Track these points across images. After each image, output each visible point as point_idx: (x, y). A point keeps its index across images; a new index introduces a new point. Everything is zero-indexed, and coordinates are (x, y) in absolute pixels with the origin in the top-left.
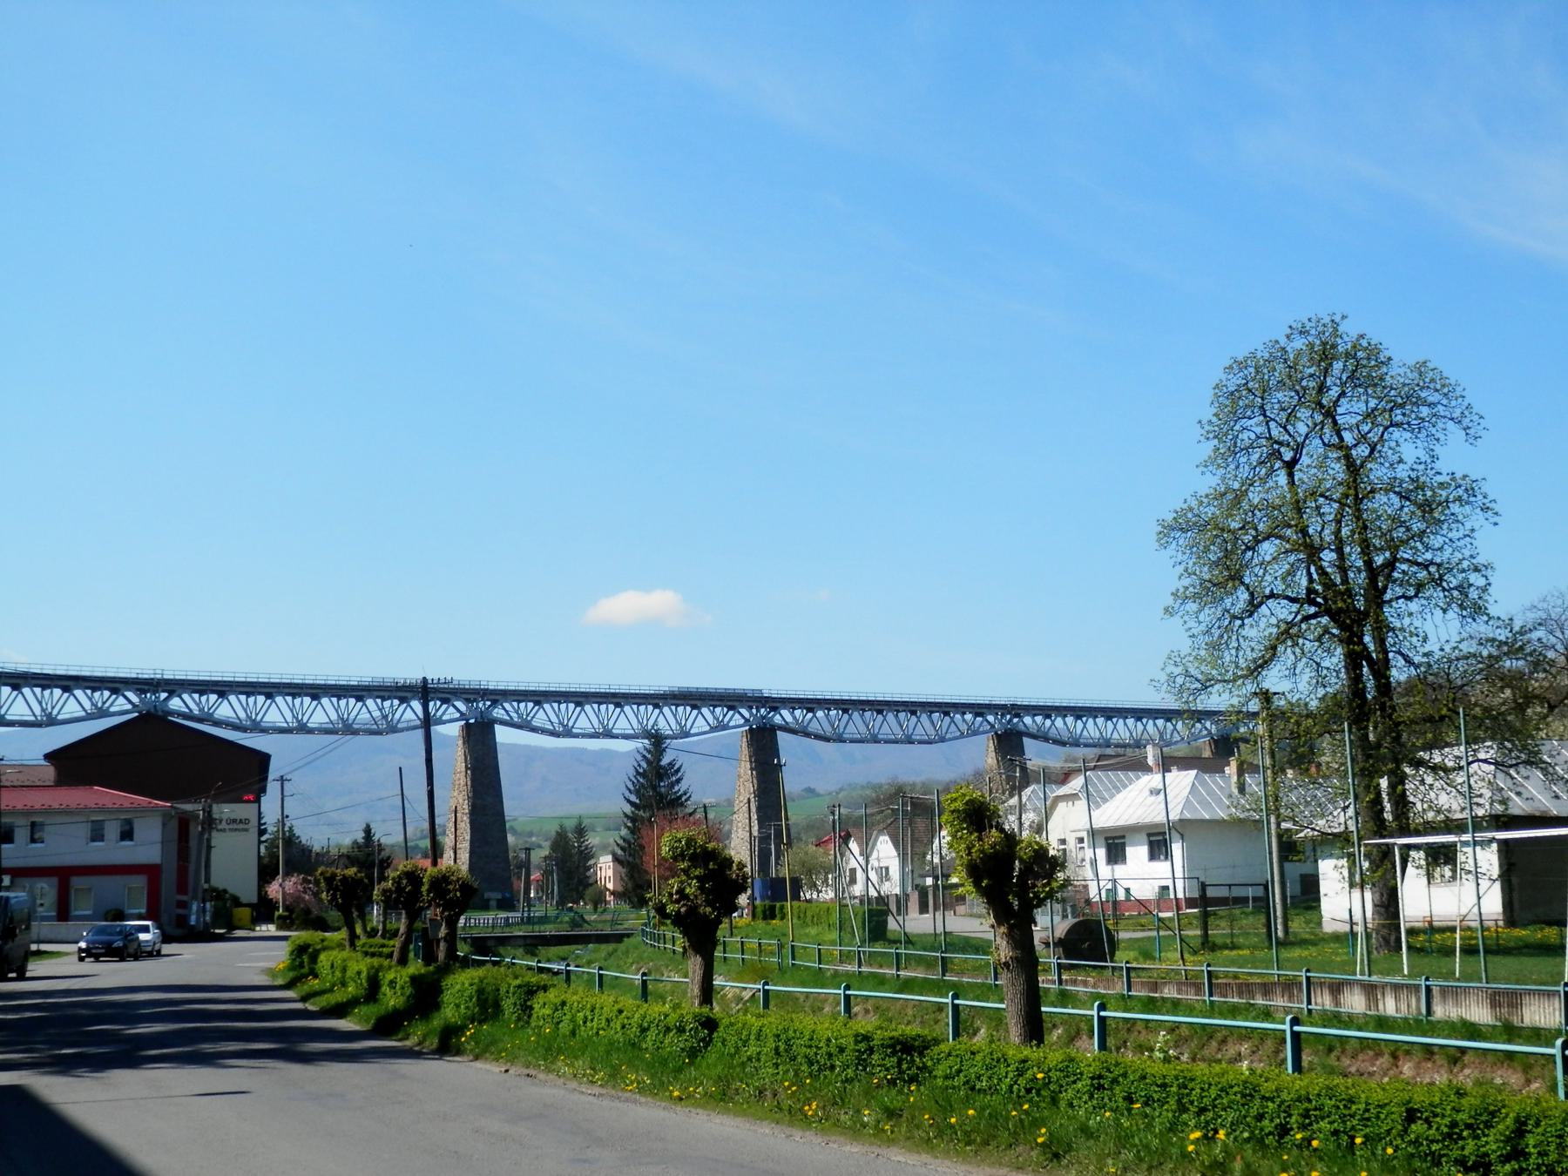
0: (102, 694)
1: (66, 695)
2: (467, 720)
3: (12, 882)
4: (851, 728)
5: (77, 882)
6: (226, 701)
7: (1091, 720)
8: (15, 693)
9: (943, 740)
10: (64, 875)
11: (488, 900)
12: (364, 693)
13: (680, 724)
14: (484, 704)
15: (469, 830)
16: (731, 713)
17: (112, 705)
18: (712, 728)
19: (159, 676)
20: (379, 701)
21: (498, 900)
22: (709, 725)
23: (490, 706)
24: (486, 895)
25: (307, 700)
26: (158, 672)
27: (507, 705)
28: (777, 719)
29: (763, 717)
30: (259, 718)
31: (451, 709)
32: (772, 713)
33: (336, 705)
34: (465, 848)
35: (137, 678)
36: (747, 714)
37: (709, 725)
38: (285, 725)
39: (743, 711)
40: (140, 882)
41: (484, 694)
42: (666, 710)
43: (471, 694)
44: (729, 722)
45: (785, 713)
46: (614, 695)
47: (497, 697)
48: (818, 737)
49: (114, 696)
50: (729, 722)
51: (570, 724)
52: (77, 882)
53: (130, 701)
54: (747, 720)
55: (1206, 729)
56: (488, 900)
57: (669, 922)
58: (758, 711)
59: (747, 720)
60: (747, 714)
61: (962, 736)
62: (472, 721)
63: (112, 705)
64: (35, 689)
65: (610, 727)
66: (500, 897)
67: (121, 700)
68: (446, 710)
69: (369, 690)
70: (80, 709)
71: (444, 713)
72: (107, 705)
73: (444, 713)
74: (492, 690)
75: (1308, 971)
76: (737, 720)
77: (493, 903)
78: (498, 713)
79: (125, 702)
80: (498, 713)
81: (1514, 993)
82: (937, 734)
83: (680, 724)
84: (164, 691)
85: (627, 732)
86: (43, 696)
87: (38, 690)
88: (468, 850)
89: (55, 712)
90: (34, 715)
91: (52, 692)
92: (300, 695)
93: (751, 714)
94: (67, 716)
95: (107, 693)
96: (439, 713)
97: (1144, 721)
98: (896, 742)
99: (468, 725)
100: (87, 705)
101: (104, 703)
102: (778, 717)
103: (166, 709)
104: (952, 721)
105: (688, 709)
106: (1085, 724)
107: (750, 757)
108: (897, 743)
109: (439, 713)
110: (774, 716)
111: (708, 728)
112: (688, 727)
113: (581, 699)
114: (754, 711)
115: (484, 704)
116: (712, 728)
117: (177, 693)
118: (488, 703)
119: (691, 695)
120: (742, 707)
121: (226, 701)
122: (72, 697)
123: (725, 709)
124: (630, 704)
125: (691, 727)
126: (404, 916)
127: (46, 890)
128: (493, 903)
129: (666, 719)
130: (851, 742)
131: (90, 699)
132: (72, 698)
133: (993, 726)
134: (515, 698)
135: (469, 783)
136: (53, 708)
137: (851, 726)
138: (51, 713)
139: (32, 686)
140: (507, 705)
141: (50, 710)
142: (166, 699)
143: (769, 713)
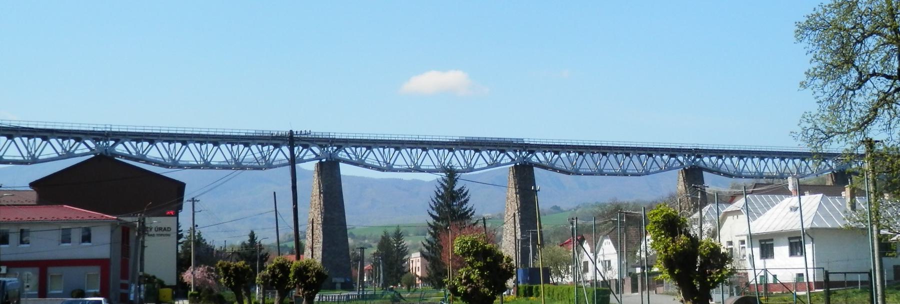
0: (69, 142)
2: (321, 160)
3: (7, 271)
5: (52, 271)
7: (749, 160)
9: (648, 173)
10: (43, 266)
11: (335, 283)
14: (332, 149)
15: (322, 235)
16: (502, 155)
17: (76, 149)
18: (489, 165)
20: (260, 146)
21: (342, 284)
22: (57, 152)
23: (336, 150)
24: (334, 280)
28: (534, 159)
29: (524, 158)
32: (530, 155)
36: (513, 156)
37: (57, 152)
39: (511, 154)
40: (95, 271)
41: (332, 141)
42: (430, 152)
45: (539, 155)
46: (422, 142)
48: (562, 171)
49: (78, 143)
52: (52, 271)
54: (513, 160)
55: (829, 166)
56: (335, 283)
59: (513, 160)
60: (513, 156)
61: (661, 170)
63: (76, 149)
65: (419, 164)
66: (343, 281)
69: (158, 136)
70: (161, 157)
72: (73, 149)
74: (337, 139)
76: (507, 160)
77: (338, 285)
78: (342, 155)
79: (85, 147)
80: (342, 155)
82: (644, 169)
84: (112, 140)
85: (430, 168)
88: (321, 249)
89: (37, 154)
90: (23, 156)
91: (35, 141)
92: (205, 142)
93: (516, 156)
95: (73, 141)
96: (499, 159)
97: (786, 160)
98: (615, 174)
102: (534, 157)
103: (113, 152)
104: (654, 160)
105: (473, 152)
106: (745, 162)
107: (515, 185)
109: (499, 159)
110: (531, 157)
112: (473, 164)
113: (398, 145)
114: (518, 153)
115: (332, 149)
116: (489, 165)
118: (335, 148)
120: (510, 151)
122: (13, 143)
123: (498, 152)
128: (338, 285)
130: (584, 175)
131: (61, 145)
132: (49, 144)
133: (682, 164)
134: (354, 144)
135: (322, 203)
136: (36, 151)
137: (371, 156)
138: (34, 155)
139: (21, 136)
140: (348, 150)
141: (33, 153)
142: (114, 145)
143: (528, 155)
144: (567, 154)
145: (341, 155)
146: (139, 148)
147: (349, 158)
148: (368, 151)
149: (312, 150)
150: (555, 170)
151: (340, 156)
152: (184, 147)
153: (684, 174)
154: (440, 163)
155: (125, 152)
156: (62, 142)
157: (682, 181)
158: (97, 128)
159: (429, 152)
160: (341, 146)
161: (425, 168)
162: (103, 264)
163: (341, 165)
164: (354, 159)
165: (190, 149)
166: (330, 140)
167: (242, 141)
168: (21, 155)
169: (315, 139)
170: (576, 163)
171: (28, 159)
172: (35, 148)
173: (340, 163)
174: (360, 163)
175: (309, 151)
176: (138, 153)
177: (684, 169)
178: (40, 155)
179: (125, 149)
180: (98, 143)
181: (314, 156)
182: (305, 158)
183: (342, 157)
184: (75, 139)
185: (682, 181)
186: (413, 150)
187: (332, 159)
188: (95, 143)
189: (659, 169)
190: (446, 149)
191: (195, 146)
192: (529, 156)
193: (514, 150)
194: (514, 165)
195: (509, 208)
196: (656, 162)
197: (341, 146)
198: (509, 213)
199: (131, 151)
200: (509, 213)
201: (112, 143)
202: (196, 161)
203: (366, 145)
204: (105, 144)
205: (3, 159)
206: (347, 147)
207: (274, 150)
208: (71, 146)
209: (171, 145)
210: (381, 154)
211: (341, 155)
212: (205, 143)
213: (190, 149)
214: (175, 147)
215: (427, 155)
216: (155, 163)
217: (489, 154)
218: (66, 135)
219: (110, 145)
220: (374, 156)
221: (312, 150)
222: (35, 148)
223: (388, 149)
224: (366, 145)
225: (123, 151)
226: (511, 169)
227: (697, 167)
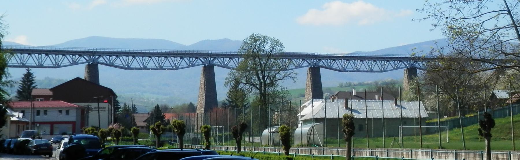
0: (76, 57)
1: (64, 57)
3: (39, 125)
4: (349, 67)
5: (55, 126)
6: (118, 59)
8: (47, 56)
9: (385, 71)
10: (52, 124)
12: (135, 55)
13: (369, 67)
14: (316, 60)
16: (401, 63)
17: (196, 62)
18: (296, 67)
19: (95, 50)
23: (318, 61)
25: (179, 59)
26: (95, 49)
27: (324, 61)
28: (417, 65)
29: (412, 64)
30: (130, 65)
31: (403, 64)
32: (415, 63)
33: (55, 58)
34: (203, 110)
35: (88, 51)
38: (156, 67)
39: (405, 62)
40: (70, 126)
41: (211, 55)
42: (378, 62)
43: (206, 55)
44: (400, 66)
47: (215, 57)
48: (337, 70)
49: (80, 57)
50: (400, 66)
51: (162, 65)
52: (55, 126)
53: (86, 59)
54: (309, 64)
57: (121, 126)
58: (410, 62)
60: (406, 64)
61: (394, 69)
62: (206, 65)
63: (196, 62)
64: (53, 55)
65: (359, 68)
67: (82, 58)
68: (401, 64)
69: (50, 52)
71: (400, 65)
72: (77, 60)
73: (400, 65)
75: (456, 151)
76: (403, 65)
78: (321, 63)
79: (84, 59)
80: (321, 63)
81: (447, 152)
83: (369, 67)
84: (97, 55)
86: (297, 61)
87: (54, 55)
90: (53, 64)
92: (160, 57)
93: (408, 64)
94: (182, 67)
96: (399, 65)
98: (367, 72)
99: (205, 66)
100: (188, 63)
101: (76, 60)
102: (417, 64)
103: (97, 62)
105: (386, 62)
107: (310, 77)
108: (354, 72)
109: (399, 65)
110: (416, 64)
111: (69, 64)
113: (134, 55)
114: (409, 62)
116: (71, 63)
117: (82, 56)
119: (291, 55)
120: (85, 55)
121: (118, 59)
123: (399, 62)
124: (379, 60)
125: (61, 64)
126: (178, 137)
127: (48, 129)
129: (31, 60)
131: (72, 59)
133: (406, 66)
134: (173, 56)
136: (59, 62)
138: (58, 63)
139: (69, 55)
140: (324, 61)
141: (58, 62)
142: (213, 60)
143: (414, 63)
144: (394, 61)
145: (216, 62)
146: (74, 58)
147: (419, 67)
148: (134, 58)
149: (84, 58)
150: (333, 69)
151: (215, 63)
152: (182, 59)
153: (407, 71)
154: (383, 68)
155: (103, 62)
156: (72, 57)
157: (406, 75)
158: (355, 55)
159: (350, 62)
160: (215, 58)
161: (362, 70)
162: (73, 123)
163: (99, 65)
164: (108, 63)
165: (337, 63)
166: (209, 55)
167: (346, 59)
168: (52, 64)
169: (186, 54)
170: (371, 67)
171: (56, 66)
172: (59, 60)
173: (320, 68)
174: (111, 65)
175: (403, 63)
176: (110, 62)
177: (408, 68)
178: (61, 64)
179: (104, 60)
180: (90, 57)
181: (85, 61)
182: (303, 66)
183: (216, 63)
184: (302, 59)
185: (406, 75)
186: (298, 60)
187: (316, 66)
188: (88, 57)
189: (393, 68)
190: (372, 60)
191: (155, 58)
192: (414, 64)
193: (407, 61)
194: (310, 67)
195: (307, 90)
196: (391, 64)
197: (215, 58)
198: (307, 93)
199: (325, 64)
200: (307, 93)
201: (97, 57)
202: (156, 66)
203: (180, 56)
204: (93, 57)
205: (43, 66)
206: (324, 60)
207: (399, 63)
208: (77, 59)
209: (143, 58)
210: (173, 61)
211: (216, 62)
212: (41, 54)
213: (337, 63)
214: (24, 57)
215: (363, 64)
216: (120, 67)
217: (394, 63)
218: (160, 55)
219: (96, 58)
220: (336, 65)
221: (84, 58)
222: (59, 60)
223: (384, 61)
224: (180, 56)
225: (217, 63)
226: (309, 69)
227: (414, 68)
